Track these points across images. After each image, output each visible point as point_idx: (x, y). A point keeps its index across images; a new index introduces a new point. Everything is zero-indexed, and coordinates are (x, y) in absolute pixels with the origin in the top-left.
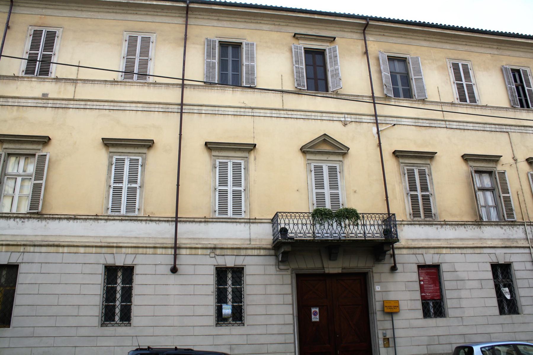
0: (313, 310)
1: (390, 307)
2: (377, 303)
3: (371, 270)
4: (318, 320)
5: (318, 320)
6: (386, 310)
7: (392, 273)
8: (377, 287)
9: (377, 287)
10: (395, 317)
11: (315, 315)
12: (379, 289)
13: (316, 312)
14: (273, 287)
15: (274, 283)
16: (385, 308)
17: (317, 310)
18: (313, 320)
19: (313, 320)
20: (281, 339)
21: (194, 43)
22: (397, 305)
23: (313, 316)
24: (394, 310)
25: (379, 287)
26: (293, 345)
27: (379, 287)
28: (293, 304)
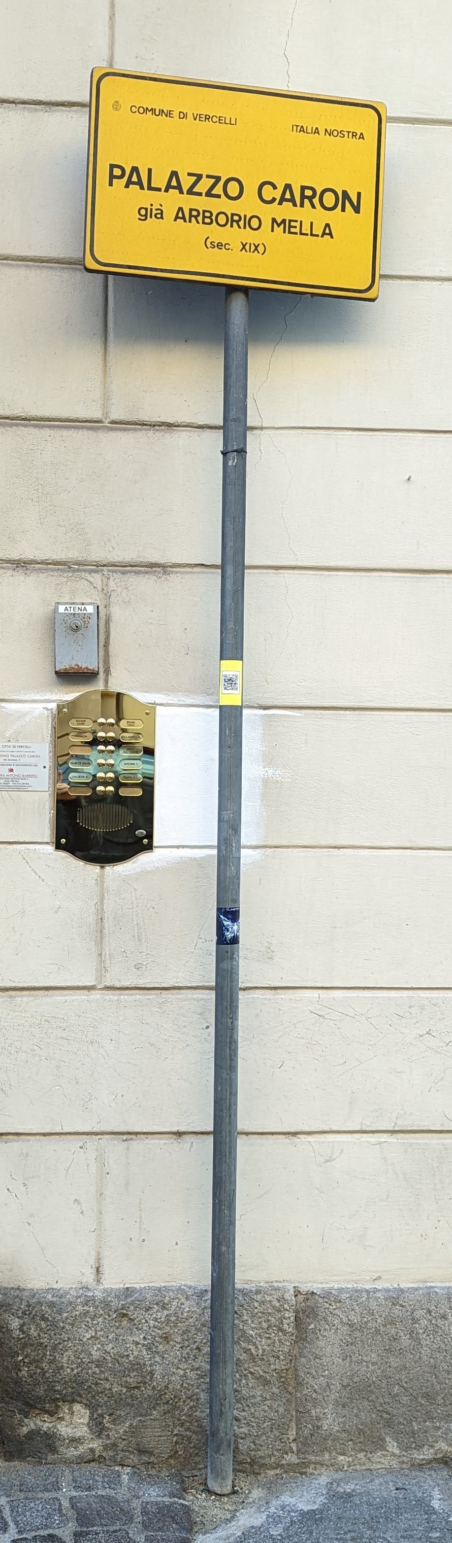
1: (206, 195)
10: (287, 381)
24: (280, 261)
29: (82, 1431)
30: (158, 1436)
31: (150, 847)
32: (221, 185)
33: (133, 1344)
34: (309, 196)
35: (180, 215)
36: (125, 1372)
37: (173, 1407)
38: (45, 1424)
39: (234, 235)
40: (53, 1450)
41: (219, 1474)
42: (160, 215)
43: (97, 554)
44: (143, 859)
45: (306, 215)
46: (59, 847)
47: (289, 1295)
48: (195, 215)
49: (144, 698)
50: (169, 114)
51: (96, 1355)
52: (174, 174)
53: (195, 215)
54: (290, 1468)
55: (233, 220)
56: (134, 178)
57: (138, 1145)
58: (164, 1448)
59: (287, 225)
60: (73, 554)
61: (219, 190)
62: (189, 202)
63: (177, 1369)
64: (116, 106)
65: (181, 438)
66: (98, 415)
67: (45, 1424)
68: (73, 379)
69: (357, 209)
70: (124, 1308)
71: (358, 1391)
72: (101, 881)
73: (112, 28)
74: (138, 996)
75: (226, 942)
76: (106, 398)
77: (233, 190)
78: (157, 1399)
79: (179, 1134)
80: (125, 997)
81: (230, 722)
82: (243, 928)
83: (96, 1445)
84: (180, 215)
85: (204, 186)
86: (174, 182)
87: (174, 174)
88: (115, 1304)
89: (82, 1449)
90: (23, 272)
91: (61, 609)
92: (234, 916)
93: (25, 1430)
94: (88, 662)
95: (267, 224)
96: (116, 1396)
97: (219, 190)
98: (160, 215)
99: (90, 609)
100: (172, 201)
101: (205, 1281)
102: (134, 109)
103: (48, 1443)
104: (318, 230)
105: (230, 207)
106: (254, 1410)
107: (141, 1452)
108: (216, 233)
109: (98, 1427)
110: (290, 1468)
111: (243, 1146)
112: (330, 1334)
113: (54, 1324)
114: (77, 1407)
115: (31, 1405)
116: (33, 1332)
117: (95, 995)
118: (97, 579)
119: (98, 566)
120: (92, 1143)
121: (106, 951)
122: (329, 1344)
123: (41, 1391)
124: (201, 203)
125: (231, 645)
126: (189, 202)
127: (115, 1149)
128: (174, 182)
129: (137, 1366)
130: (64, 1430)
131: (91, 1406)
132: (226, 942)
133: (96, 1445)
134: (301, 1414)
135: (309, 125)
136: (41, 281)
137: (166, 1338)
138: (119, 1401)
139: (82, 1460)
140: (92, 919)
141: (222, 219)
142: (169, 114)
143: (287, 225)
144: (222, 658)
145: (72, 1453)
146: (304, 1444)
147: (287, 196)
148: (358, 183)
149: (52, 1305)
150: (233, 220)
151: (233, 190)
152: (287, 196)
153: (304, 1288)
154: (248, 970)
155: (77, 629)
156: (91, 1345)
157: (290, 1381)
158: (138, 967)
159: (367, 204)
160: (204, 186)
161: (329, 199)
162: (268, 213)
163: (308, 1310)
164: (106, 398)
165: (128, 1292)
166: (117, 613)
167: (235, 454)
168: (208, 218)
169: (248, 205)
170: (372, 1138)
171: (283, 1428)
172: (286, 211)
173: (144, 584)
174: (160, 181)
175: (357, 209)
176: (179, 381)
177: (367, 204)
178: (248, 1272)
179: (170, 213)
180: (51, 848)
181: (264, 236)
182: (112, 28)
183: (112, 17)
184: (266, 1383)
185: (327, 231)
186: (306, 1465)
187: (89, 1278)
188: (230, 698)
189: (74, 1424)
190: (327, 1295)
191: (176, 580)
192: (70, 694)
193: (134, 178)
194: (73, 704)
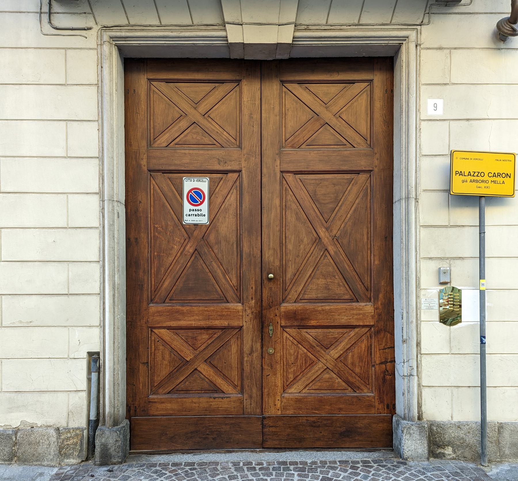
0: (189, 184)
1: (476, 176)
2: (425, 164)
3: (412, 35)
4: (204, 220)
5: (204, 220)
6: (460, 187)
7: (502, 45)
8: (431, 102)
9: (431, 102)
10: (493, 215)
11: (193, 201)
12: (439, 113)
13: (198, 192)
14: (29, 92)
15: (31, 80)
16: (457, 180)
17: (203, 185)
18: (188, 220)
19: (188, 220)
20: (55, 278)
21: (476, 423)
22: (506, 168)
23: (187, 206)
24: (492, 190)
25: (440, 103)
26: (95, 301)
27: (440, 103)
28: (101, 158)
29: (451, 453)
30: (468, 454)
31: (461, 322)
32: (480, 174)
33: (461, 434)
34: (499, 175)
35: (471, 181)
36: (460, 440)
37: (471, 448)
38: (442, 451)
39: (483, 185)
40: (444, 456)
41: (484, 461)
42: (467, 181)
43: (448, 256)
44: (459, 325)
45: (499, 179)
46: (440, 322)
47: (496, 423)
48: (474, 181)
49: (459, 288)
50: (468, 159)
51: (453, 436)
52: (469, 172)
53: (474, 181)
54: (498, 462)
55: (482, 181)
56: (461, 174)
57: (460, 389)
58: (469, 457)
59: (494, 182)
60: (442, 256)
61: (479, 175)
62: (473, 178)
63: (473, 439)
64: (457, 158)
65: (466, 229)
66: (447, 224)
67: (442, 451)
68: (442, 216)
69: (510, 177)
70: (459, 426)
71: (513, 445)
72: (450, 329)
73: (449, 137)
74: (459, 355)
75: (482, 343)
76: (449, 220)
77: (482, 174)
78: (467, 446)
79: (469, 387)
80: (456, 356)
81: (482, 294)
82: (486, 340)
83: (454, 456)
84: (471, 181)
85: (476, 174)
86: (469, 174)
87: (469, 172)
88: (457, 425)
89: (451, 457)
90: (430, 193)
91: (442, 269)
92: (484, 337)
93: (438, 452)
94: (448, 280)
95: (490, 182)
96: (458, 445)
97: (479, 175)
98: (467, 181)
99: (448, 268)
100: (469, 178)
101: (479, 420)
102: (490, 175)
103: (444, 455)
104: (501, 182)
105: (482, 178)
106: (491, 448)
107: (464, 457)
108: (479, 185)
109: (454, 452)
110: (498, 462)
111: (488, 390)
112: (507, 432)
113: (443, 429)
114: (449, 447)
115: (439, 447)
116: (439, 430)
117: (449, 355)
118: (448, 261)
119: (448, 258)
120: (450, 388)
121: (452, 345)
122: (506, 434)
123: (441, 443)
124: (476, 178)
125: (482, 276)
126: (473, 178)
127: (455, 390)
128: (469, 174)
129: (463, 438)
130: (446, 452)
131: (453, 447)
132: (482, 343)
133: (454, 456)
134: (500, 450)
135: (499, 159)
136: (433, 195)
137: (469, 432)
138: (459, 446)
139: (451, 459)
140: (448, 338)
141: (480, 181)
142: (468, 159)
143: (494, 182)
144: (480, 279)
145: (449, 457)
146: (501, 456)
147: (494, 175)
148: (510, 172)
149: (443, 424)
150: (482, 181)
151: (482, 174)
152: (494, 175)
153: (499, 422)
154: (488, 350)
155: (445, 273)
156: (451, 434)
157: (498, 442)
158: (459, 349)
159: (512, 176)
160: (476, 174)
161: (504, 175)
162: (490, 179)
163: (501, 427)
164: (449, 220)
165: (460, 422)
166: (452, 268)
167: (482, 233)
168: (477, 181)
169: (486, 178)
170: (514, 388)
171: (496, 453)
172: (494, 179)
173: (458, 262)
174: (466, 174)
175: (510, 177)
176: (468, 216)
177: (512, 176)
178: (491, 417)
179: (469, 181)
180: (438, 322)
181: (490, 184)
182: (449, 137)
183: (449, 135)
184: (492, 443)
185: (503, 183)
186: (502, 461)
187: (450, 419)
188: (482, 288)
189: (449, 451)
190: (505, 423)
191: (466, 261)
192: (442, 287)
193: (461, 174)
194: (443, 290)
